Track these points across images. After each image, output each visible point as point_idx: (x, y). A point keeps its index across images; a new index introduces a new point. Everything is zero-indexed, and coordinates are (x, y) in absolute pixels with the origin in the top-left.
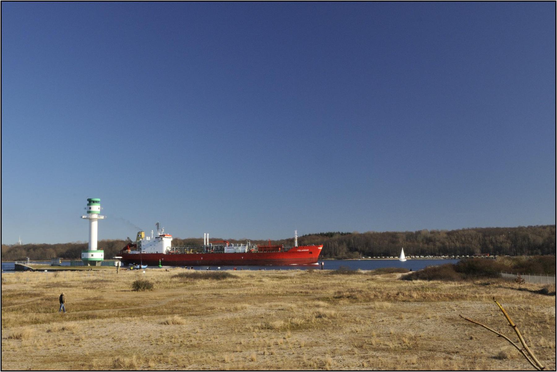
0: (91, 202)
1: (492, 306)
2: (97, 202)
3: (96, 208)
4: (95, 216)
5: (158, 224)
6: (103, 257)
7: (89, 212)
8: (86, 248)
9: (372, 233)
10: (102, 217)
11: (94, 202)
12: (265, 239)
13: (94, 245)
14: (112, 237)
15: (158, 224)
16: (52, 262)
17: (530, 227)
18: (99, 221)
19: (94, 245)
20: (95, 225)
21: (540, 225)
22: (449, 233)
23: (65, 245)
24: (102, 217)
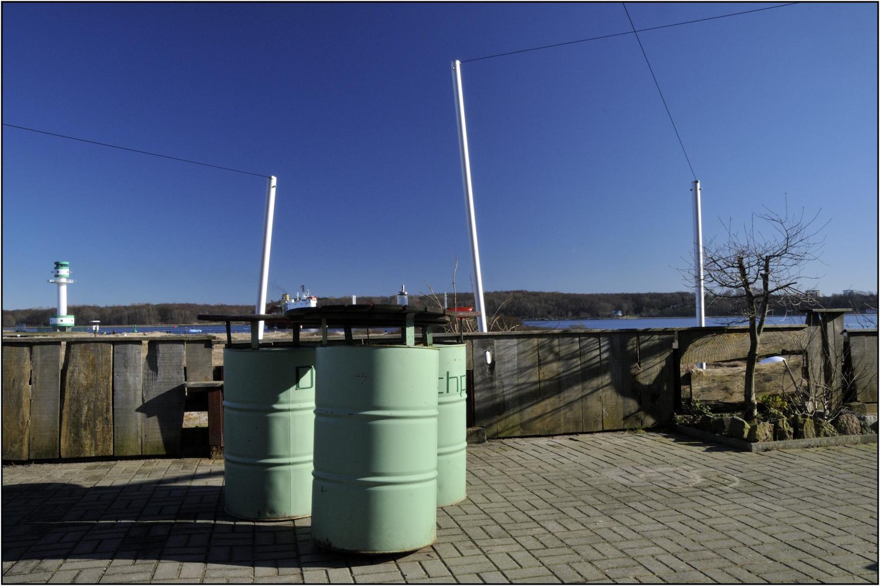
0: (58, 265)
1: (863, 386)
2: (65, 265)
3: (64, 272)
4: (64, 280)
5: (303, 287)
6: (73, 323)
7: (57, 276)
8: (54, 313)
9: (868, 294)
10: (71, 281)
11: (62, 265)
12: (240, 304)
13: (64, 310)
14: (79, 303)
15: (303, 287)
16: (17, 328)
17: (496, 293)
18: (68, 285)
19: (64, 310)
20: (64, 290)
21: (504, 290)
22: (421, 298)
23: (26, 311)
24: (71, 281)
